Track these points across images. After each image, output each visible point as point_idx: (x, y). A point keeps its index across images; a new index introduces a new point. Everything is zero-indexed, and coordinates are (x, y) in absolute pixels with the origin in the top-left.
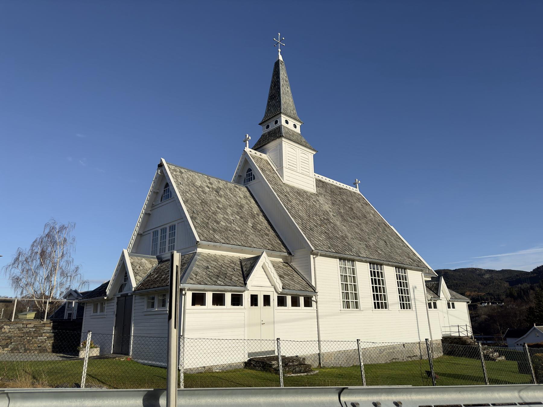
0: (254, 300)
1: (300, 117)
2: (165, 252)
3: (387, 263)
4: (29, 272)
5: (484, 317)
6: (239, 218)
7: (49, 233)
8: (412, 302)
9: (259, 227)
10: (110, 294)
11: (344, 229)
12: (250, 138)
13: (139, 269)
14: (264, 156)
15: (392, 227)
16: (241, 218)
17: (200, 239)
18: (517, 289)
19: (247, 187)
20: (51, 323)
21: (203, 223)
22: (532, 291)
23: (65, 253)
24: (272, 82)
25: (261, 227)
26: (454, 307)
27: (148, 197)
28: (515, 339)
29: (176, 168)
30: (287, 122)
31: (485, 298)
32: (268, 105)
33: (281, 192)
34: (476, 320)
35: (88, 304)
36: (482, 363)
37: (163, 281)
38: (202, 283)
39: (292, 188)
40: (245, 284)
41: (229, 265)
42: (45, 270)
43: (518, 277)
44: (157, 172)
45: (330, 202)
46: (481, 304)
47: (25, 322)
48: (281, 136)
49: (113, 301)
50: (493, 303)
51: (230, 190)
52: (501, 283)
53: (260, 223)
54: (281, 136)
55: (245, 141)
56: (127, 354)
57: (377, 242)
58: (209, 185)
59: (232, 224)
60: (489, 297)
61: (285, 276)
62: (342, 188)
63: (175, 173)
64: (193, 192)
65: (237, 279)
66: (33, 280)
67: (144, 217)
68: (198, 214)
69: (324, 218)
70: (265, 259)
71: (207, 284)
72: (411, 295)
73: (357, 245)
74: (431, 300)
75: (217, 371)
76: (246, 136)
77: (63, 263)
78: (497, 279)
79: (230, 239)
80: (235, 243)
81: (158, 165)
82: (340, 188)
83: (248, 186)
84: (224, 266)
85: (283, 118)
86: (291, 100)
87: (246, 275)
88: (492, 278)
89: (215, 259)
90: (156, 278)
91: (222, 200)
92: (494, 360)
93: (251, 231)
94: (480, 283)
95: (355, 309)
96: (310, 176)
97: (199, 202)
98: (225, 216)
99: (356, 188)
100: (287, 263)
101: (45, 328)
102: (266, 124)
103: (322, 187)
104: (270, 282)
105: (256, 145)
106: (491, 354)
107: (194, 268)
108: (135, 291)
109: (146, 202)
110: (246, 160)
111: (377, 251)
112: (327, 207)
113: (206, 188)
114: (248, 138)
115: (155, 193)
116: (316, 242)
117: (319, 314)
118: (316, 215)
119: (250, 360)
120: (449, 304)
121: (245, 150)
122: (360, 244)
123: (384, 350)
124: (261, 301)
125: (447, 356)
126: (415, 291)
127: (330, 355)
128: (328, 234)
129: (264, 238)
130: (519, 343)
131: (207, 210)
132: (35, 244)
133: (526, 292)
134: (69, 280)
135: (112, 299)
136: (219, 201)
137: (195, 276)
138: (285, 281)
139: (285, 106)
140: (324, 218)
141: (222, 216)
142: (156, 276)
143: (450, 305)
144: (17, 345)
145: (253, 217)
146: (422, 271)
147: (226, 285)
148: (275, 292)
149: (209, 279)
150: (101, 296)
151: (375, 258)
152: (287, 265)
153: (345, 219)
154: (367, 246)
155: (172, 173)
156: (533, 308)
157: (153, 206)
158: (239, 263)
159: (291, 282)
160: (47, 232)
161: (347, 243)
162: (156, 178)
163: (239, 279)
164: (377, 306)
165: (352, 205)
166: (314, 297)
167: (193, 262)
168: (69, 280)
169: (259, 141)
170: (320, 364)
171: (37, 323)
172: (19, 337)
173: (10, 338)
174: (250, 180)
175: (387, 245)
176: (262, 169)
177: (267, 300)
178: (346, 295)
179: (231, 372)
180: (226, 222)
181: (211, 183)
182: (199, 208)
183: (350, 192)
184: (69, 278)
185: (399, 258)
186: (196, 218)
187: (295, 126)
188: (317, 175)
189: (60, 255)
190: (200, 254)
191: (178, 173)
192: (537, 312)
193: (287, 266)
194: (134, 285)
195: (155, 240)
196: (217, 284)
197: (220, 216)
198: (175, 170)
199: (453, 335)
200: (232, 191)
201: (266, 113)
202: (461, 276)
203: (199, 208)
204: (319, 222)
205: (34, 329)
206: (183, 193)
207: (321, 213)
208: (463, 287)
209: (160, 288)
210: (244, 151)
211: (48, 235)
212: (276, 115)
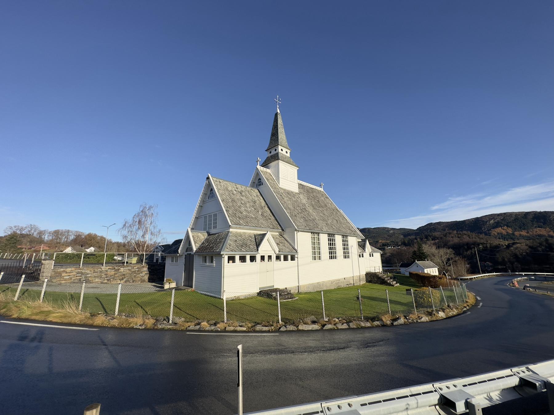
0: (263, 258)
1: (291, 145)
2: (211, 229)
3: (337, 233)
4: (132, 232)
5: (388, 254)
6: (253, 209)
7: (142, 210)
8: (350, 255)
9: (265, 214)
10: (181, 252)
11: (314, 214)
12: (260, 160)
13: (197, 239)
14: (268, 170)
15: (342, 211)
16: (255, 209)
17: (231, 223)
18: (408, 239)
19: (258, 190)
20: (147, 266)
21: (233, 213)
22: (416, 241)
23: (152, 221)
24: (273, 126)
25: (266, 214)
26: (373, 256)
27: (201, 196)
28: (405, 268)
29: (217, 180)
30: (282, 150)
31: (390, 244)
32: (271, 139)
33: (278, 193)
34: (384, 256)
35: (168, 257)
36: (387, 296)
37: (211, 249)
38: (233, 251)
39: (285, 190)
40: (258, 250)
41: (248, 239)
42: (141, 231)
43: (409, 233)
44: (205, 182)
45: (306, 198)
46: (387, 247)
47: (132, 266)
48: (278, 159)
49: (183, 257)
50: (394, 247)
51: (248, 191)
52: (399, 235)
53: (266, 212)
54: (278, 159)
55: (257, 162)
56: (192, 287)
57: (332, 221)
58: (236, 189)
59: (250, 214)
60: (392, 243)
61: (280, 244)
62: (313, 189)
63: (216, 183)
64: (227, 194)
65: (253, 247)
66: (134, 237)
67: (198, 208)
68: (230, 208)
69: (303, 208)
70: (269, 236)
71: (236, 251)
72: (350, 251)
73: (321, 224)
74: (360, 253)
75: (243, 298)
76: (258, 158)
77: (152, 227)
78: (397, 234)
79: (248, 223)
80: (251, 225)
81: (207, 178)
82: (312, 189)
83: (259, 189)
84: (245, 239)
85: (280, 148)
86: (285, 136)
87: (258, 245)
88: (394, 233)
89: (240, 235)
90: (207, 246)
91: (244, 198)
92: (393, 286)
93: (261, 217)
94: (387, 236)
95: (319, 260)
96: (295, 182)
97: (230, 200)
98: (246, 208)
99: (321, 188)
100: (281, 235)
101: (144, 269)
102: (270, 151)
103: (302, 188)
104: (272, 248)
105: (264, 163)
106: (392, 283)
107: (229, 241)
108: (195, 252)
109: (200, 199)
110: (258, 174)
111: (332, 227)
112: (304, 201)
113: (235, 191)
114: (259, 160)
115: (205, 194)
116: (298, 224)
117: (299, 264)
118: (298, 206)
119: (260, 292)
120: (370, 254)
121: (257, 167)
122: (323, 223)
123: (334, 282)
124: (266, 258)
125: (368, 283)
126: (352, 248)
127: (304, 286)
128: (305, 218)
129: (268, 221)
130: (407, 271)
131: (235, 205)
132: (135, 217)
133: (412, 240)
134: (155, 237)
135: (182, 255)
136: (242, 199)
137: (229, 247)
138: (280, 247)
139: (281, 140)
140: (303, 208)
141: (244, 209)
142: (207, 244)
143: (371, 255)
144: (129, 278)
145: (262, 208)
146: (356, 237)
147: (247, 251)
148: (274, 253)
149: (237, 248)
150: (175, 253)
151: (331, 231)
152: (281, 236)
153: (315, 208)
154: (326, 224)
155: (214, 183)
156: (416, 251)
157: (204, 201)
158: (254, 237)
159: (284, 247)
160: (141, 210)
161: (315, 223)
162: (205, 185)
163: (254, 247)
164: (331, 258)
165: (319, 199)
166: (296, 255)
167: (228, 237)
168: (155, 237)
169: (265, 161)
170: (299, 291)
171: (139, 266)
172: (129, 274)
173: (124, 275)
174: (260, 185)
175: (337, 222)
176: (267, 179)
177: (270, 257)
178: (314, 248)
179: (250, 299)
180: (246, 212)
181: (237, 188)
182: (231, 204)
183: (318, 190)
184: (155, 236)
185: (344, 230)
186: (229, 211)
187: (287, 152)
188: (299, 181)
189: (150, 223)
190: (231, 233)
191: (218, 183)
192: (418, 253)
193: (281, 237)
194: (195, 249)
195: (205, 222)
196: (242, 251)
197: (243, 209)
198: (216, 181)
199: (371, 271)
200: (249, 192)
201: (270, 144)
202: (377, 232)
203: (231, 204)
204: (300, 211)
205: (137, 270)
206: (221, 195)
207: (301, 205)
208: (378, 237)
209: (209, 253)
210: (257, 168)
211: (142, 211)
212: (275, 146)
